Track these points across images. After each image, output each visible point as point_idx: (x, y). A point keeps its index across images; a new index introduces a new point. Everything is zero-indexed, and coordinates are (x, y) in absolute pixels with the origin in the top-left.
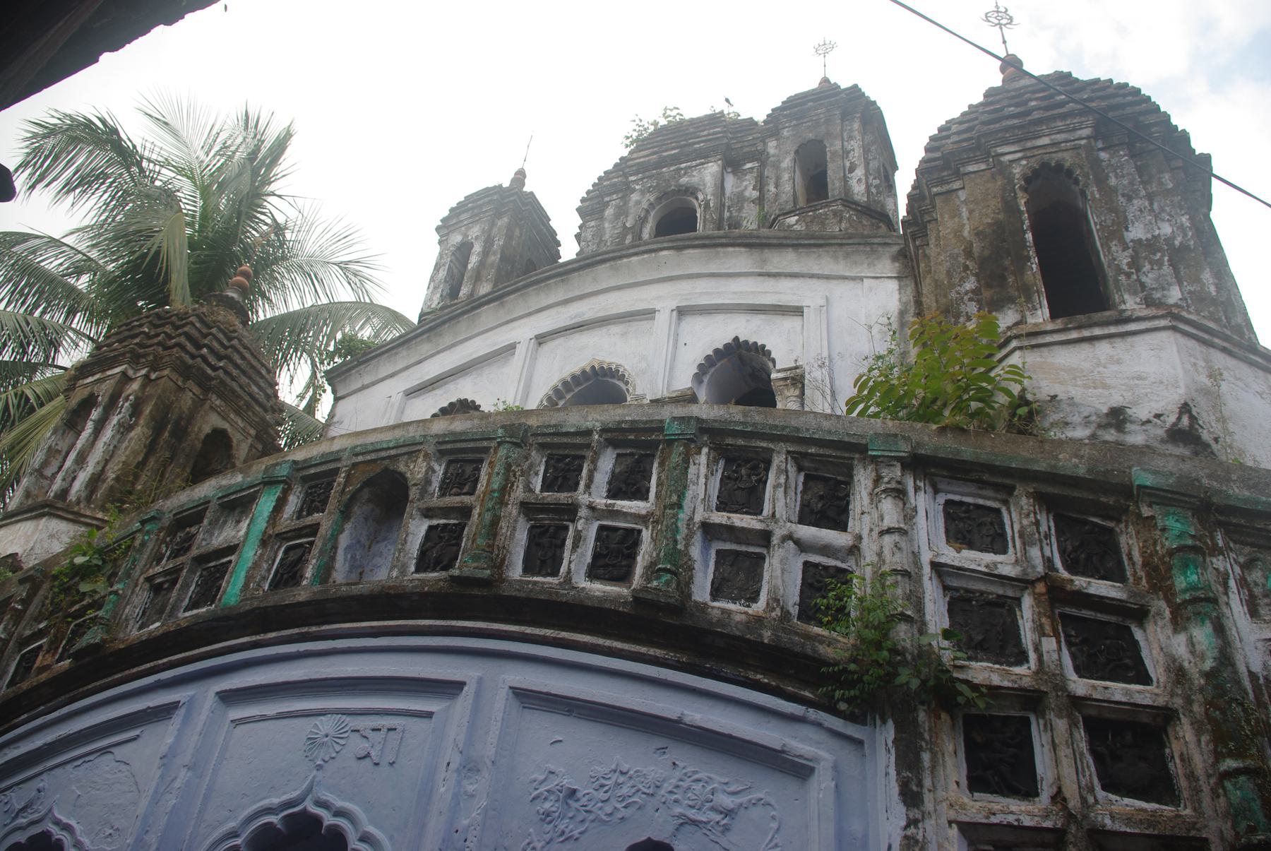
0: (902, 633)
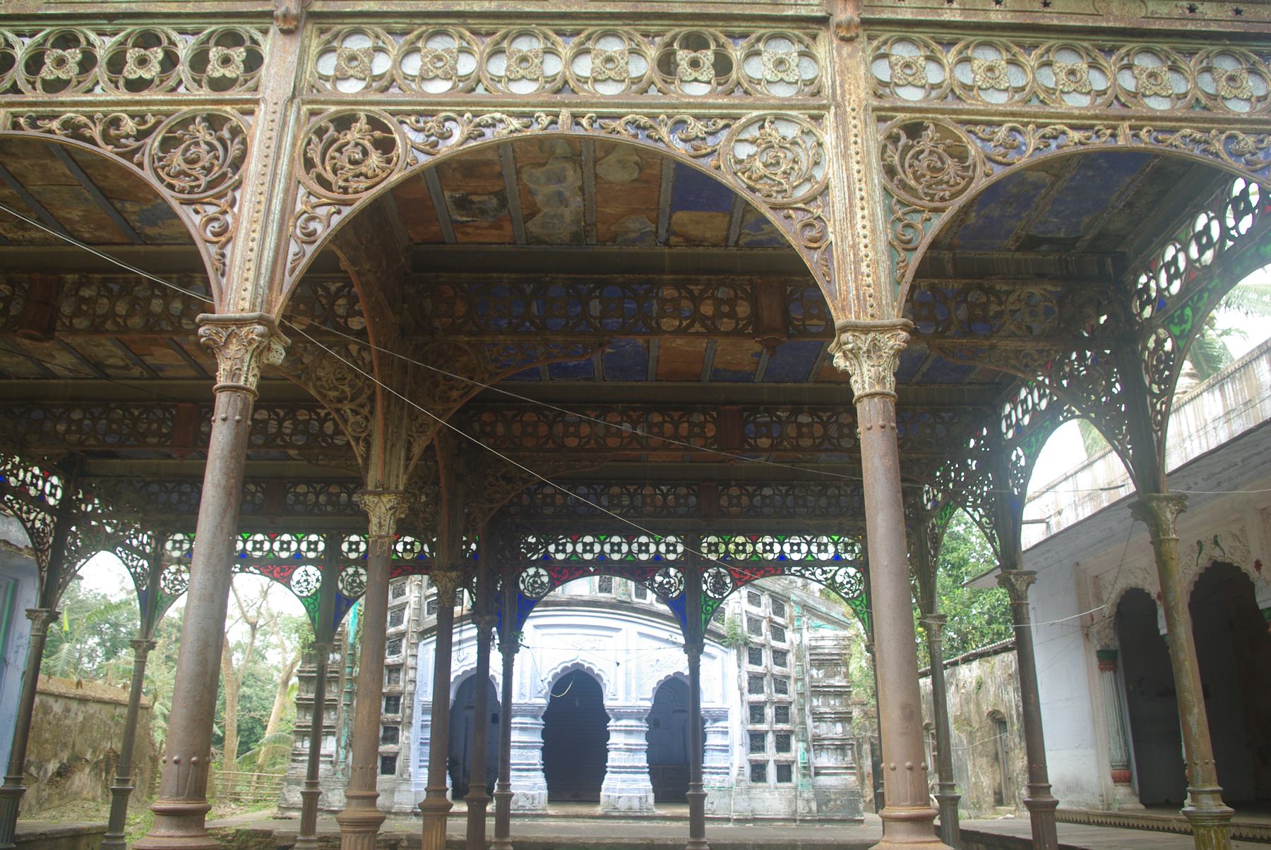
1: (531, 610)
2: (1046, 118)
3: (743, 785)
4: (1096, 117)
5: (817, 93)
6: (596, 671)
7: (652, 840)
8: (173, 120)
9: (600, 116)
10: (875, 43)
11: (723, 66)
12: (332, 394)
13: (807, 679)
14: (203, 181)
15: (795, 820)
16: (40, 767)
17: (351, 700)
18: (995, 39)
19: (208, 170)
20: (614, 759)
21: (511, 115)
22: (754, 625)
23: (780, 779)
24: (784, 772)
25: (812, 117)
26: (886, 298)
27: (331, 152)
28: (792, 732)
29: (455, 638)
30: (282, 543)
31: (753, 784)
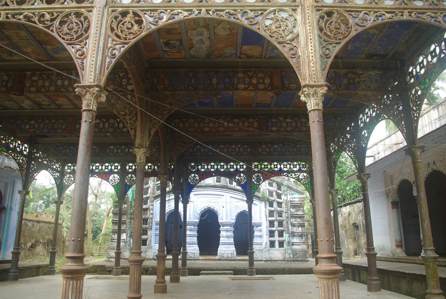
0: (265, 196)
3: (267, 249)
4: (396, 9)
6: (216, 210)
7: (236, 268)
8: (63, 14)
12: (122, 113)
13: (289, 212)
14: (75, 36)
15: (285, 261)
16: (25, 245)
17: (131, 221)
20: (222, 240)
22: (271, 193)
23: (280, 247)
24: (281, 244)
25: (293, 10)
27: (120, 25)
28: (284, 230)
30: (106, 166)
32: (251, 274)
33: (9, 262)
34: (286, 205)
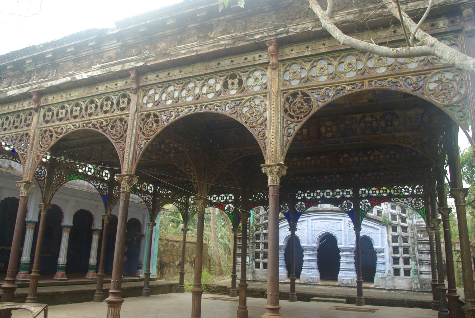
0: (387, 219)
1: (298, 218)
2: (338, 83)
3: (390, 277)
4: (355, 80)
5: (266, 88)
6: (334, 235)
7: (349, 296)
8: (112, 121)
9: (208, 105)
10: (285, 67)
11: (240, 82)
12: (188, 170)
13: (416, 237)
14: (119, 136)
15: (412, 291)
16: (173, 263)
17: (253, 245)
18: (324, 57)
19: (120, 133)
20: (342, 266)
21: (186, 108)
22: (394, 217)
23: (406, 275)
24: (407, 273)
25: (264, 96)
26: (279, 154)
27: (146, 125)
28: (410, 257)
29: (280, 226)
30: (222, 197)
31: (395, 277)
32: (360, 304)
33: (142, 280)
34: (412, 229)
